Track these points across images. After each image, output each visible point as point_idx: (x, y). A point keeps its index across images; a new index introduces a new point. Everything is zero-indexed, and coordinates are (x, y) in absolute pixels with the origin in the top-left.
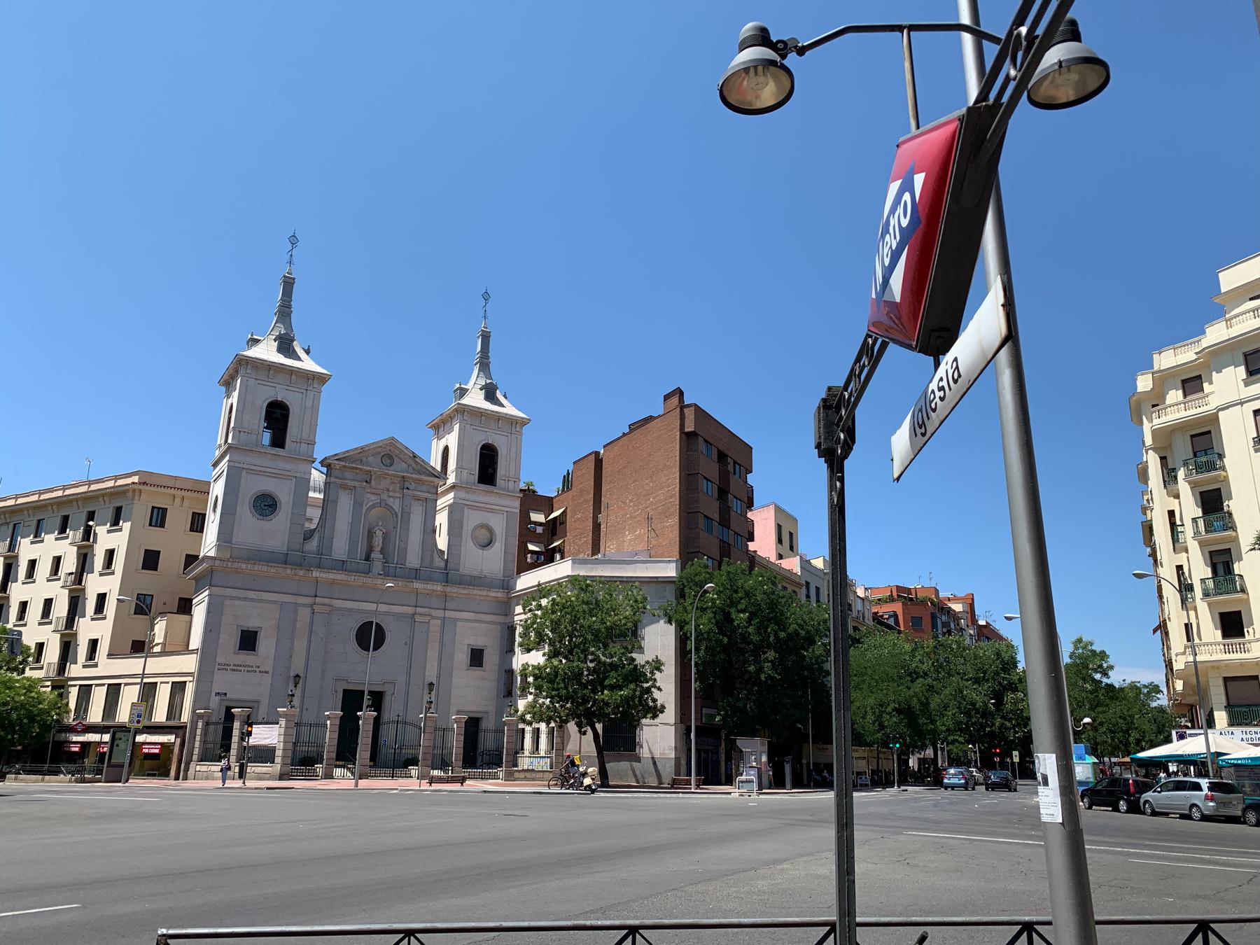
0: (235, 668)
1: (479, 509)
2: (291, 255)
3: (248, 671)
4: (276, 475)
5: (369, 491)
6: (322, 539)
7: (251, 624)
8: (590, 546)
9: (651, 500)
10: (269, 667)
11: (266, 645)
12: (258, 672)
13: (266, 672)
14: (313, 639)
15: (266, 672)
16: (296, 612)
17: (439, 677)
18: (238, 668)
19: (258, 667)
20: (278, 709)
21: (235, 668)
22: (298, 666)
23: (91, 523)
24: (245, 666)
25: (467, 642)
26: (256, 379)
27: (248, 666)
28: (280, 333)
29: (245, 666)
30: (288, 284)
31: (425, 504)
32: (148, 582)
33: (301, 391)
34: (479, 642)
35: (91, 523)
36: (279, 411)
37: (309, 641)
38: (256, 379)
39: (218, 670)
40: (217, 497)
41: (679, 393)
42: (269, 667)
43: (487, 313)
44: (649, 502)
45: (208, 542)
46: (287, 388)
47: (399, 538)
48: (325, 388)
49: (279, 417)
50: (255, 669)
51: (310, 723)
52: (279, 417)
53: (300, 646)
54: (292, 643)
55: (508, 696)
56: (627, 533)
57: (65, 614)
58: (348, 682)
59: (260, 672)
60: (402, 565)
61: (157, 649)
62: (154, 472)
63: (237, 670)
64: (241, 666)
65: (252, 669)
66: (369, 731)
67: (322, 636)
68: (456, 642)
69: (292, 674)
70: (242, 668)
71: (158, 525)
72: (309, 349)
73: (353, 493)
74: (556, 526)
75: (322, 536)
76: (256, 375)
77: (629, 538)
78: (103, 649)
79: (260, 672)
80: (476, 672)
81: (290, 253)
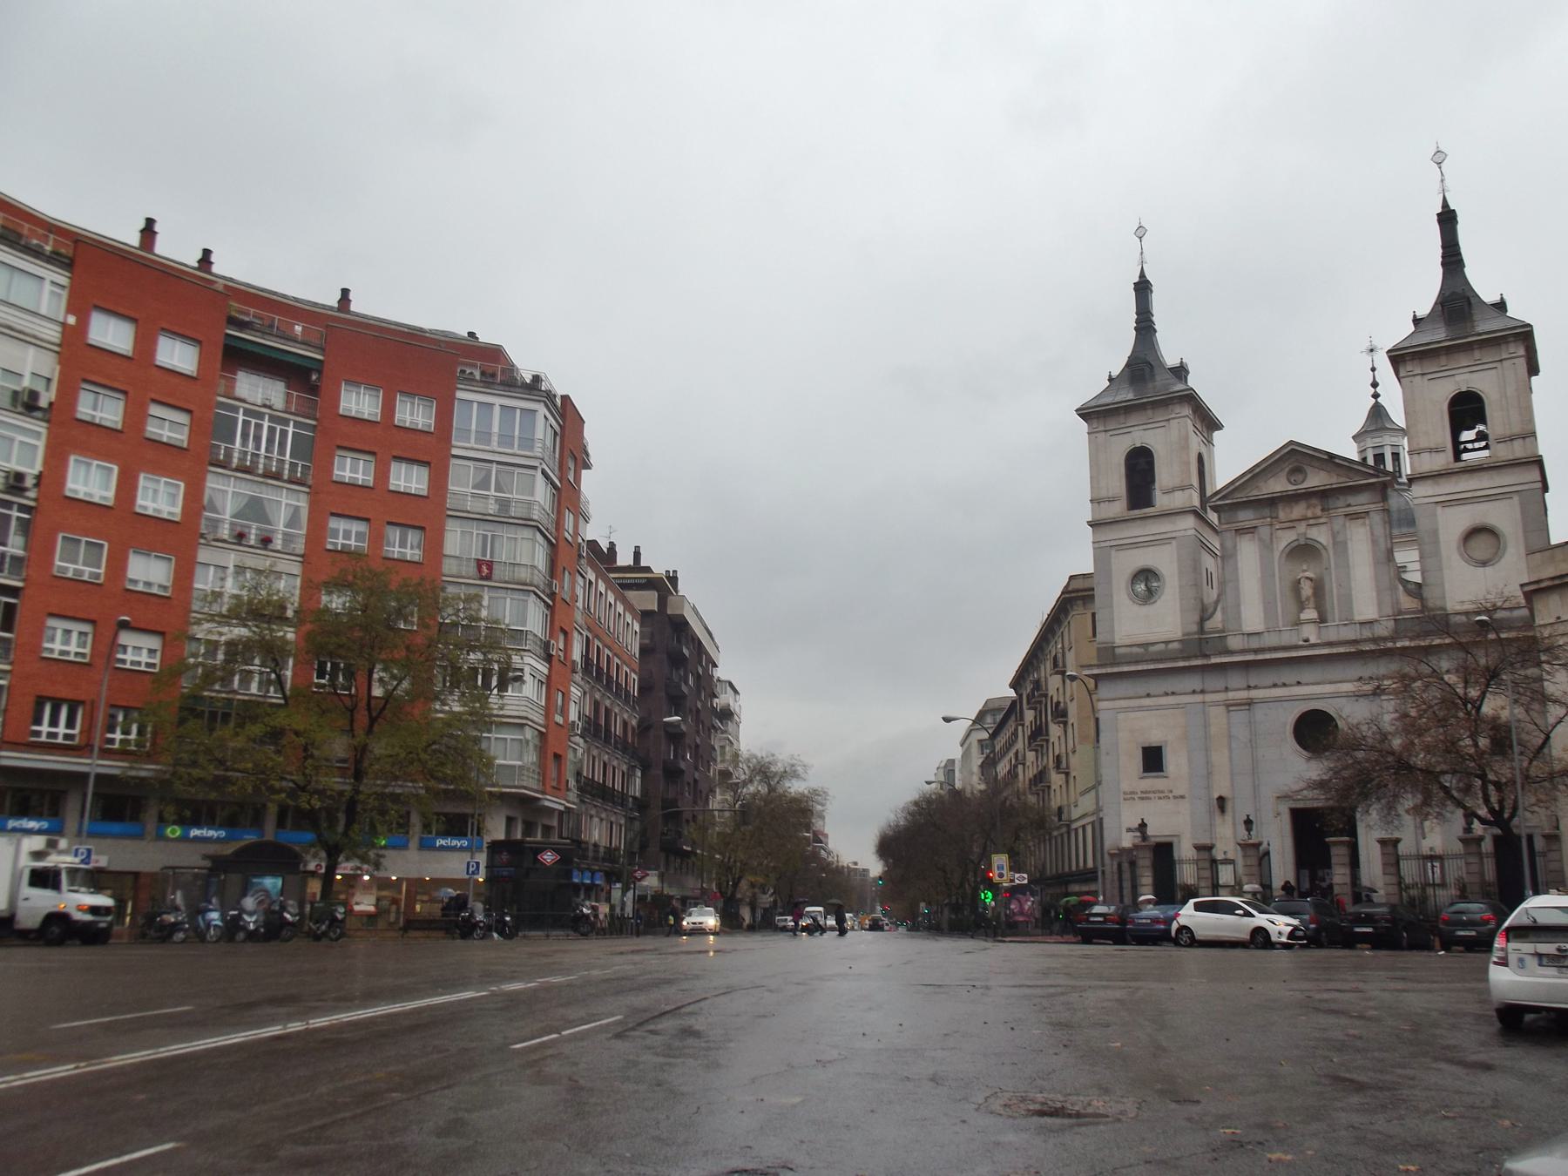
7: (1154, 739)
11: (1172, 761)
13: (1182, 797)
15: (1182, 797)
19: (1171, 792)
24: (1154, 792)
26: (1106, 431)
29: (1154, 792)
39: (1125, 799)
46: (1145, 427)
59: (1175, 797)
64: (1149, 792)
79: (1175, 797)
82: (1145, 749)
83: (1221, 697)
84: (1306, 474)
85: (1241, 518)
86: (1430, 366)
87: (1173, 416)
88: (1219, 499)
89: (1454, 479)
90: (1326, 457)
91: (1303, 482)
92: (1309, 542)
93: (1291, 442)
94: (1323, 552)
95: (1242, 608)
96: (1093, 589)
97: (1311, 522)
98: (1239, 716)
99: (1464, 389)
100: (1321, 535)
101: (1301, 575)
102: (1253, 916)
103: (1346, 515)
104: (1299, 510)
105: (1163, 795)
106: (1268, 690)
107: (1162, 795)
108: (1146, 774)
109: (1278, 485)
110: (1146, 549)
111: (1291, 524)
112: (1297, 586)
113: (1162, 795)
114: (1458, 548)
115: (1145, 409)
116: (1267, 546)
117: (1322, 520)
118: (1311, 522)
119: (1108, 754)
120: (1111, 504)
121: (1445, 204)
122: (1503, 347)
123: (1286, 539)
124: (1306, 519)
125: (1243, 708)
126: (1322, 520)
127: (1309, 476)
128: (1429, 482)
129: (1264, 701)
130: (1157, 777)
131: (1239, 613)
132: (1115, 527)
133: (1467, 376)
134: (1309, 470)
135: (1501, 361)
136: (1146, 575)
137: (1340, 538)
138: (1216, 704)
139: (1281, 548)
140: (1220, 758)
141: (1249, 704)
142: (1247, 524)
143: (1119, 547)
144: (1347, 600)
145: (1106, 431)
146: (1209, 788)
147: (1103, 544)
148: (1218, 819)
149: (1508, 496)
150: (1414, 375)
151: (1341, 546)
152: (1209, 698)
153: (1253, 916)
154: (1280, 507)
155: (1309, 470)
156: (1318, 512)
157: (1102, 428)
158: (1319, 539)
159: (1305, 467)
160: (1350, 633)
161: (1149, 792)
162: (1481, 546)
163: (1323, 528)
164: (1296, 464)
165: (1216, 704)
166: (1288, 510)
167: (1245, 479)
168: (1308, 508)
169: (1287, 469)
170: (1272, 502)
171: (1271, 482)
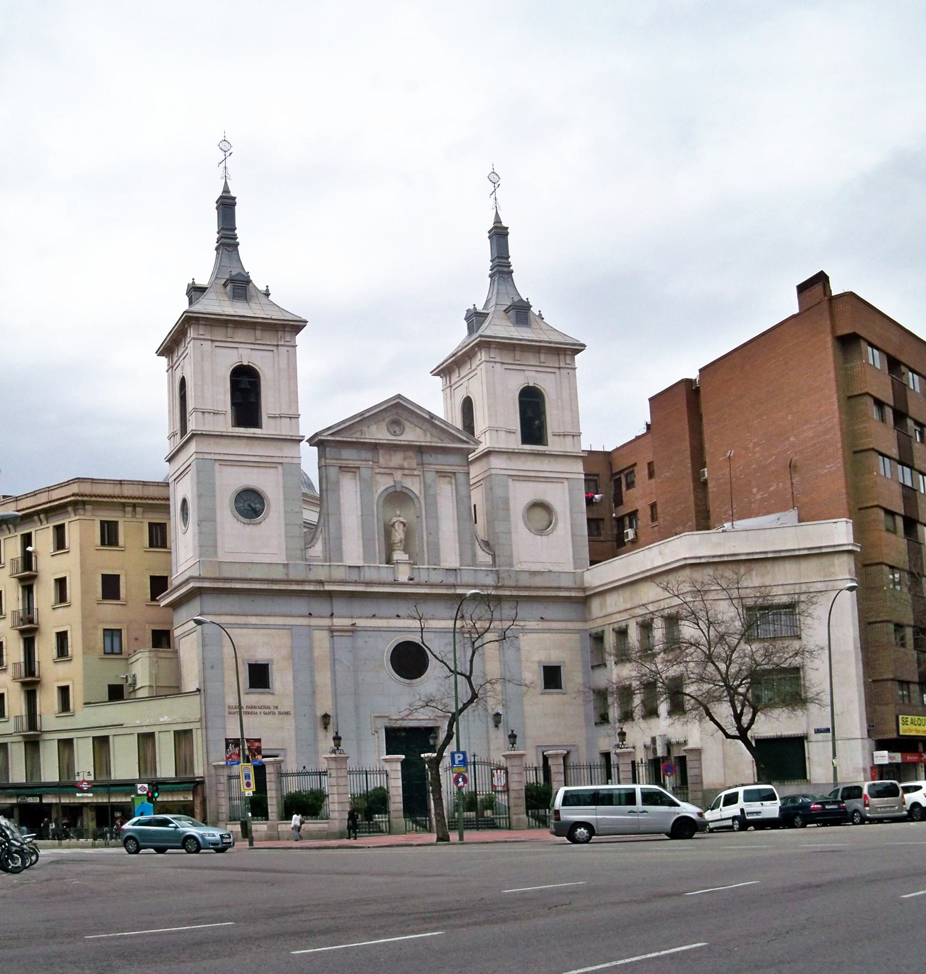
0: (250, 710)
1: (528, 479)
2: (225, 168)
3: (265, 714)
4: (257, 465)
5: (377, 472)
6: (327, 541)
7: (261, 656)
8: (692, 515)
9: (792, 439)
10: (287, 704)
11: (280, 679)
12: (277, 713)
13: (287, 713)
14: (337, 668)
15: (287, 713)
16: (310, 638)
17: (335, 704)
18: (253, 710)
19: (277, 707)
20: (422, 755)
21: (250, 710)
22: (325, 705)
23: (29, 549)
24: (260, 708)
25: (536, 658)
26: (502, 363)
27: (265, 707)
28: (513, 301)
29: (260, 708)
30: (499, 234)
31: (453, 481)
32: (110, 612)
33: (552, 370)
34: (554, 658)
35: (29, 549)
36: (247, 379)
37: (334, 672)
38: (212, 341)
39: (230, 713)
40: (184, 501)
41: (821, 279)
42: (287, 704)
43: (229, 170)
44: (787, 443)
45: (182, 559)
46: (253, 347)
47: (427, 529)
48: (300, 338)
49: (248, 387)
50: (272, 710)
51: (588, 764)
52: (248, 387)
53: (323, 678)
54: (312, 675)
55: (601, 723)
56: (755, 490)
57: (22, 660)
58: (390, 720)
59: (280, 713)
60: (435, 565)
61: (141, 694)
62: (94, 478)
63: (252, 713)
64: (255, 707)
65: (270, 711)
66: (269, 782)
67: (348, 664)
68: (523, 659)
69: (320, 713)
70: (258, 711)
71: (159, 545)
72: (267, 290)
73: (358, 477)
74: (621, 492)
75: (327, 537)
76: (501, 359)
77: (758, 497)
78: (75, 699)
79: (280, 713)
80: (553, 698)
81: (223, 165)
82: (268, 664)
83: (326, 622)
84: (404, 429)
85: (344, 457)
86: (219, 334)
87: (282, 343)
88: (332, 434)
89: (523, 458)
90: (427, 417)
91: (402, 434)
92: (404, 490)
93: (399, 396)
94: (416, 500)
95: (344, 541)
96: (168, 499)
97: (406, 472)
98: (343, 642)
99: (245, 363)
100: (414, 486)
101: (395, 519)
102: (678, 805)
103: (437, 472)
104: (397, 459)
105: (268, 711)
106: (369, 620)
107: (267, 710)
108: (252, 690)
109: (379, 433)
110: (250, 469)
111: (387, 471)
112: (388, 531)
113: (267, 710)
114: (523, 517)
115: (255, 329)
116: (366, 487)
117: (416, 473)
118: (406, 472)
119: (212, 667)
120: (216, 416)
121: (498, 220)
122: (280, 334)
123: (384, 484)
124: (402, 468)
125: (347, 634)
126: (416, 473)
127: (407, 429)
128: (505, 457)
129: (366, 630)
130: (262, 693)
131: (341, 544)
132: (224, 441)
133: (533, 374)
134: (407, 425)
135: (559, 368)
136: (540, 506)
137: (431, 492)
138: (320, 628)
139: (380, 491)
140: (323, 678)
141: (352, 631)
142: (351, 463)
143: (224, 463)
144: (435, 549)
145: (502, 363)
146: (313, 706)
147: (207, 456)
148: (321, 733)
149: (274, 465)
150: (496, 362)
151: (432, 501)
152: (314, 622)
153: (678, 805)
154: (381, 452)
155: (407, 425)
156: (414, 463)
157: (498, 359)
158: (412, 489)
159: (402, 420)
160: (436, 578)
161: (255, 707)
162: (540, 516)
163: (416, 480)
164: (396, 417)
165: (320, 628)
166: (387, 457)
167: (356, 420)
168: (405, 459)
169: (388, 420)
170: (375, 447)
171: (374, 428)
